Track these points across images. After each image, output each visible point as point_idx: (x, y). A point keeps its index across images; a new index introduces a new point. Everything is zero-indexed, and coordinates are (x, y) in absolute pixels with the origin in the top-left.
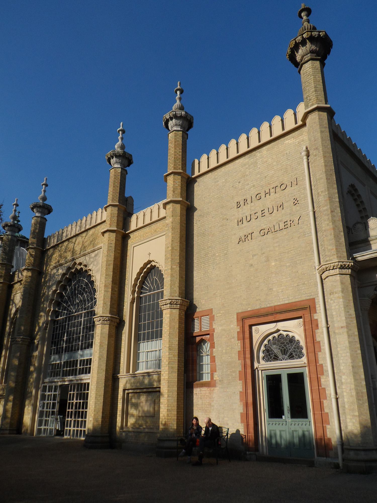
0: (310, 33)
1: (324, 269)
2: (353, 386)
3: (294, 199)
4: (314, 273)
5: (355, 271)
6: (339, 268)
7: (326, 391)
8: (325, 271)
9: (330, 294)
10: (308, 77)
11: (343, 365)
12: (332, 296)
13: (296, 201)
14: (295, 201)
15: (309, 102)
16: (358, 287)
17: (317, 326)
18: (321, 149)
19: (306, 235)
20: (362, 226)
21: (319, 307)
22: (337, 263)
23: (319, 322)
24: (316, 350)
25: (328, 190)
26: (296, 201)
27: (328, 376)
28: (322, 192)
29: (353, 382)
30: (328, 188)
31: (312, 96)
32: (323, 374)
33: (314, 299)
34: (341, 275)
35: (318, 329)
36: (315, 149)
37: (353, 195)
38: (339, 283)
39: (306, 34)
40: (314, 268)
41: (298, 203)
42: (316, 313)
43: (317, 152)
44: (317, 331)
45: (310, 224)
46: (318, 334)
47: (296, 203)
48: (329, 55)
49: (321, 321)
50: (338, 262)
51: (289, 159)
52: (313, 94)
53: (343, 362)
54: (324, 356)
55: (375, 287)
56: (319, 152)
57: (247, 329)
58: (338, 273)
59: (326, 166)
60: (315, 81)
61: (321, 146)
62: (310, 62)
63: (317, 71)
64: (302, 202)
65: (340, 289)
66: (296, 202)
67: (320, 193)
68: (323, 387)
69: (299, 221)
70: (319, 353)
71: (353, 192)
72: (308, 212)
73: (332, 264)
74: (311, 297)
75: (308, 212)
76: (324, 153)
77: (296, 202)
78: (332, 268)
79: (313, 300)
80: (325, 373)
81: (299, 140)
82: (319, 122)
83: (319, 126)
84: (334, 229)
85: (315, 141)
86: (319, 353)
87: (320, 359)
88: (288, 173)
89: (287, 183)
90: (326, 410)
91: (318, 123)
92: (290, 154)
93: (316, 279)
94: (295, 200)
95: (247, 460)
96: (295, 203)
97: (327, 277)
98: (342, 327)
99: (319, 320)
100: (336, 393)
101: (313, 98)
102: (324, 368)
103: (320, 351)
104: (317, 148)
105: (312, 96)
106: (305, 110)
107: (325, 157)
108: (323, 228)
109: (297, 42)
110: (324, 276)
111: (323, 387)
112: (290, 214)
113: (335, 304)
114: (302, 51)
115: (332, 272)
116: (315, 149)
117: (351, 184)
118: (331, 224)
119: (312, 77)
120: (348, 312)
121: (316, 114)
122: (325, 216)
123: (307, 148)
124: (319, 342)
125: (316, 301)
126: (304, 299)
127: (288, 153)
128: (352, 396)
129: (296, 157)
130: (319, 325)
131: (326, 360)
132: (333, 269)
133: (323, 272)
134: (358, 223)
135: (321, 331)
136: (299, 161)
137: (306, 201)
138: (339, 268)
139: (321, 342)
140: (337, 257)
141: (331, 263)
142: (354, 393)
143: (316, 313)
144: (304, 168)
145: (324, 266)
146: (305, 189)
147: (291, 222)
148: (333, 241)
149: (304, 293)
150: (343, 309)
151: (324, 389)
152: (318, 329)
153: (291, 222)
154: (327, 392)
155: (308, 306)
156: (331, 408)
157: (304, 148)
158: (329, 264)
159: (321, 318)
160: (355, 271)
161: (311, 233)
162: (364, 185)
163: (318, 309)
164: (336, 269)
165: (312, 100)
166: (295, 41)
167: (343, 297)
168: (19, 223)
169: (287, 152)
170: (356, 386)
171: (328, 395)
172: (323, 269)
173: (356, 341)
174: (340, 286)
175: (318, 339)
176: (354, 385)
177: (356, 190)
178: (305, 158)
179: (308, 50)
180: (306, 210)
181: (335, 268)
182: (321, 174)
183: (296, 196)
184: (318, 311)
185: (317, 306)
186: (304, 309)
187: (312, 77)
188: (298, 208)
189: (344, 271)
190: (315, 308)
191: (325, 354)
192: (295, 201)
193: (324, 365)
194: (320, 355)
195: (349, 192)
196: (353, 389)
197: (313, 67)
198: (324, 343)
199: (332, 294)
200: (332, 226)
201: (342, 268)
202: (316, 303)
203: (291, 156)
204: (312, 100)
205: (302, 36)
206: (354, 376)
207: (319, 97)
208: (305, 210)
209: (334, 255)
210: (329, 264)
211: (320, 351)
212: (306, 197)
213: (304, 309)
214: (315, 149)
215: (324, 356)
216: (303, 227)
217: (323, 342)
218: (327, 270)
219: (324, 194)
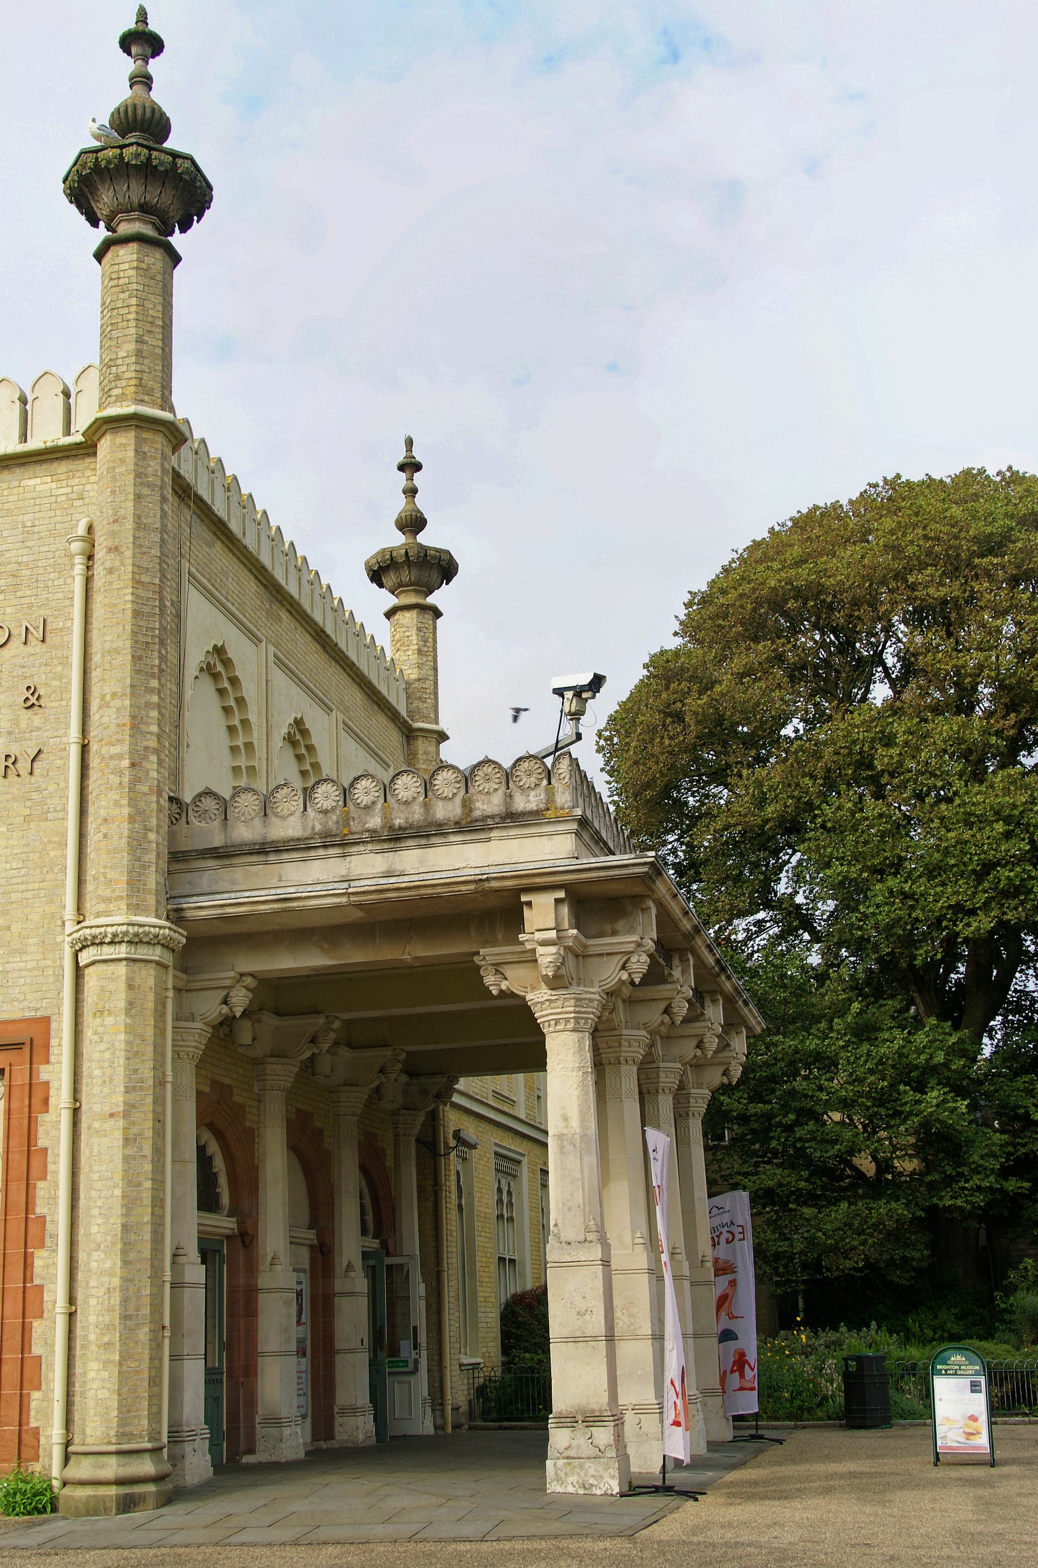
0: (146, 151)
1: (86, 939)
2: (116, 1281)
3: (28, 688)
4: (59, 939)
5: (173, 951)
6: (128, 942)
7: (45, 1294)
8: (88, 946)
9: (95, 1016)
10: (122, 296)
11: (100, 1221)
12: (98, 1021)
13: (32, 694)
14: (30, 697)
15: (113, 384)
16: (177, 990)
17: (46, 1101)
18: (129, 553)
19: (50, 816)
20: (217, 807)
21: (60, 1045)
22: (124, 928)
23: (52, 1092)
24: (34, 1173)
25: (133, 695)
26: (32, 694)
27: (56, 1251)
28: (114, 695)
29: (118, 1271)
30: (132, 686)
31: (124, 368)
32: (42, 1245)
33: (46, 1021)
34: (131, 964)
35: (47, 1111)
36: (110, 549)
37: (216, 677)
38: (122, 985)
39: (133, 149)
40: (59, 923)
41: (40, 706)
42: (47, 1061)
43: (117, 563)
44: (41, 1117)
45: (67, 781)
46: (44, 1128)
47: (33, 705)
48: (198, 222)
49: (59, 1089)
50: (128, 924)
51: (29, 544)
52: (128, 361)
53: (100, 1214)
54: (53, 1193)
55: (224, 993)
56: (122, 564)
57: (940, 1473)
58: (124, 956)
59: (136, 614)
60: (141, 317)
61: (131, 546)
62: (133, 246)
63: (152, 283)
64: (53, 704)
65: (122, 1004)
66: (33, 700)
67: (108, 698)
68: (37, 1282)
69: (35, 764)
70: (40, 1184)
71: (220, 668)
72: (65, 740)
73: (110, 930)
74: (39, 1014)
75: (65, 740)
76: (139, 569)
77: (32, 702)
78: (107, 940)
79: (45, 1022)
80: (48, 1241)
81: (68, 490)
82: (136, 464)
83: (132, 476)
84: (132, 819)
85: (115, 521)
86: (40, 1184)
87: (38, 1202)
88: (19, 594)
89: (12, 626)
90: (37, 1350)
91: (132, 467)
92: (36, 529)
93: (62, 958)
94: (31, 691)
95: (546, 1284)
96: (29, 703)
97: (93, 963)
98: (112, 1115)
99: (54, 1085)
100: (72, 1300)
101: (128, 375)
102: (49, 1226)
103: (44, 1178)
104: (116, 549)
105: (124, 368)
106: (101, 406)
107: (137, 583)
108: (102, 811)
109: (103, 164)
110: (85, 958)
111: (37, 1282)
112: (9, 733)
113: (103, 1047)
114: (115, 195)
115: (108, 952)
116: (110, 549)
117: (215, 646)
118: (125, 802)
119: (134, 301)
120: (136, 1071)
121: (127, 439)
122: (112, 773)
123: (90, 529)
124: (45, 1150)
125: (54, 1026)
126: (18, 1015)
127: (29, 524)
128: (110, 1309)
129: (53, 548)
130: (52, 1101)
131: (57, 1205)
132: (112, 943)
133: (84, 947)
134: (207, 793)
135: (55, 1119)
136: (59, 561)
137: (64, 703)
138: (128, 942)
139: (50, 1151)
140: (128, 906)
141: (108, 926)
142: (116, 1300)
143: (47, 1061)
144: (73, 592)
145: (88, 931)
146: (66, 662)
147: (9, 763)
148: (125, 859)
149: (22, 997)
150: (122, 1061)
151: (41, 1288)
152: (47, 1111)
153: (9, 763)
154: (46, 1298)
155: (28, 1042)
156: (50, 1346)
157: (81, 530)
158: (102, 926)
159: (60, 1079)
160: (173, 951)
161: (64, 810)
162: (256, 640)
163: (54, 1050)
164: (120, 942)
165: (124, 383)
166: (97, 158)
167: (129, 1030)
168: (425, 538)
169: (26, 517)
170: (125, 1280)
171: (47, 1306)
172: (82, 938)
173: (145, 1156)
174: (123, 995)
175: (42, 1142)
176: (121, 1277)
177: (227, 663)
178: (79, 560)
179: (136, 201)
180: (62, 732)
181: (117, 940)
182: (118, 636)
183: (36, 679)
184: (53, 1058)
185: (54, 1042)
186: (18, 1046)
187: (134, 301)
188: (37, 721)
189: (143, 952)
190: (47, 1046)
191: (56, 1186)
192: (30, 697)
193: (48, 1219)
194: (41, 1188)
195: (208, 670)
196: (114, 1289)
197: (143, 266)
198: (58, 1155)
199: (98, 1014)
200: (126, 811)
201: (135, 941)
202: (52, 1033)
203: (37, 536)
204: (124, 383)
205: (118, 151)
206: (124, 1252)
207: (145, 377)
208: (56, 734)
209: (122, 898)
210: (102, 926)
211: (44, 1178)
212: (66, 689)
213: (18, 1046)
214: (110, 550)
215: (53, 1193)
216: (44, 786)
217: (56, 1151)
218: (93, 944)
219: (117, 703)
